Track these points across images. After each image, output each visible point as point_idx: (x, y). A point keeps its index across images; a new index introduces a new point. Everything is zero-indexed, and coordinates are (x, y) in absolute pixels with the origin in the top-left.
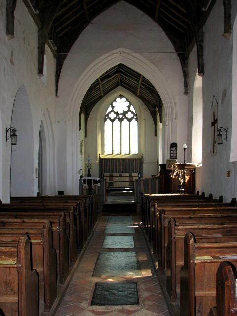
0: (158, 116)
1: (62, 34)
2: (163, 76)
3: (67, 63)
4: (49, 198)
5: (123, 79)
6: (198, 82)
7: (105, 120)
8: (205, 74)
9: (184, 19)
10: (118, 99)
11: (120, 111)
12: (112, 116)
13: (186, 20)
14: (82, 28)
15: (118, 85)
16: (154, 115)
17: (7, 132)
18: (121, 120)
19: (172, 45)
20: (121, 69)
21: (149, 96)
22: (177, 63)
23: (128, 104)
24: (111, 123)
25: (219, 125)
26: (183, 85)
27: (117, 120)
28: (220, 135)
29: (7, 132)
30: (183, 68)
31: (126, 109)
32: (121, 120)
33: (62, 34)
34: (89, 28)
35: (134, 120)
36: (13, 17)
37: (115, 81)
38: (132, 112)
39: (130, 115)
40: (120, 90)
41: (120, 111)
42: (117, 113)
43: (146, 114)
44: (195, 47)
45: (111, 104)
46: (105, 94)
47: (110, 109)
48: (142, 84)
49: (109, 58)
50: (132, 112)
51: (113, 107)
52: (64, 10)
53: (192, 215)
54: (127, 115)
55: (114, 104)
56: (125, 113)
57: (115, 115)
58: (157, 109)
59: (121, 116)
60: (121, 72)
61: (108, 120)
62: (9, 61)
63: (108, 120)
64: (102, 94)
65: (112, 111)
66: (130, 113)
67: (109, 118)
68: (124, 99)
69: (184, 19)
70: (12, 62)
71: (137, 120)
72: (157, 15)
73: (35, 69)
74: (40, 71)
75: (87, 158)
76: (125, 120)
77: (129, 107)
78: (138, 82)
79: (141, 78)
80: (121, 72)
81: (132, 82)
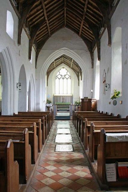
0: (80, 77)
1: (38, 41)
2: (83, 62)
3: (40, 54)
4: (32, 113)
5: (64, 60)
6: (97, 63)
7: (56, 78)
8: (101, 60)
9: (92, 36)
10: (62, 69)
11: (63, 75)
12: (59, 76)
13: (93, 36)
14: (47, 38)
15: (62, 63)
16: (78, 76)
17: (17, 84)
18: (63, 79)
19: (86, 46)
20: (63, 56)
21: (76, 68)
22: (89, 54)
23: (66, 71)
24: (62, 80)
25: (107, 82)
26: (91, 60)
27: (61, 79)
28: (106, 87)
29: (17, 84)
30: (91, 57)
31: (66, 74)
32: (63, 79)
33: (38, 41)
34: (50, 38)
35: (69, 79)
36: (21, 36)
37: (61, 61)
38: (68, 75)
39: (67, 76)
40: (63, 65)
41: (63, 75)
42: (61, 75)
43: (74, 76)
44: (97, 48)
45: (59, 71)
46: (56, 67)
47: (58, 73)
48: (73, 62)
49: (59, 52)
50: (68, 75)
51: (60, 73)
52: (40, 31)
53: (94, 119)
54: (66, 76)
55: (60, 71)
56: (65, 75)
57: (61, 76)
58: (80, 74)
59: (63, 77)
60: (64, 57)
61: (57, 79)
62: (18, 54)
63: (57, 79)
64: (55, 67)
65: (60, 74)
66: (67, 75)
67: (58, 78)
68: (65, 69)
69: (92, 36)
70: (19, 55)
71: (70, 78)
72: (80, 34)
73: (28, 58)
74: (30, 58)
75: (48, 95)
76: (65, 78)
77: (67, 73)
78: (71, 61)
79: (73, 60)
80: (64, 57)
81: (68, 61)
